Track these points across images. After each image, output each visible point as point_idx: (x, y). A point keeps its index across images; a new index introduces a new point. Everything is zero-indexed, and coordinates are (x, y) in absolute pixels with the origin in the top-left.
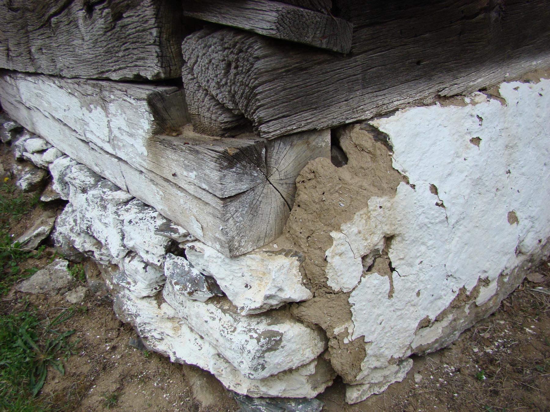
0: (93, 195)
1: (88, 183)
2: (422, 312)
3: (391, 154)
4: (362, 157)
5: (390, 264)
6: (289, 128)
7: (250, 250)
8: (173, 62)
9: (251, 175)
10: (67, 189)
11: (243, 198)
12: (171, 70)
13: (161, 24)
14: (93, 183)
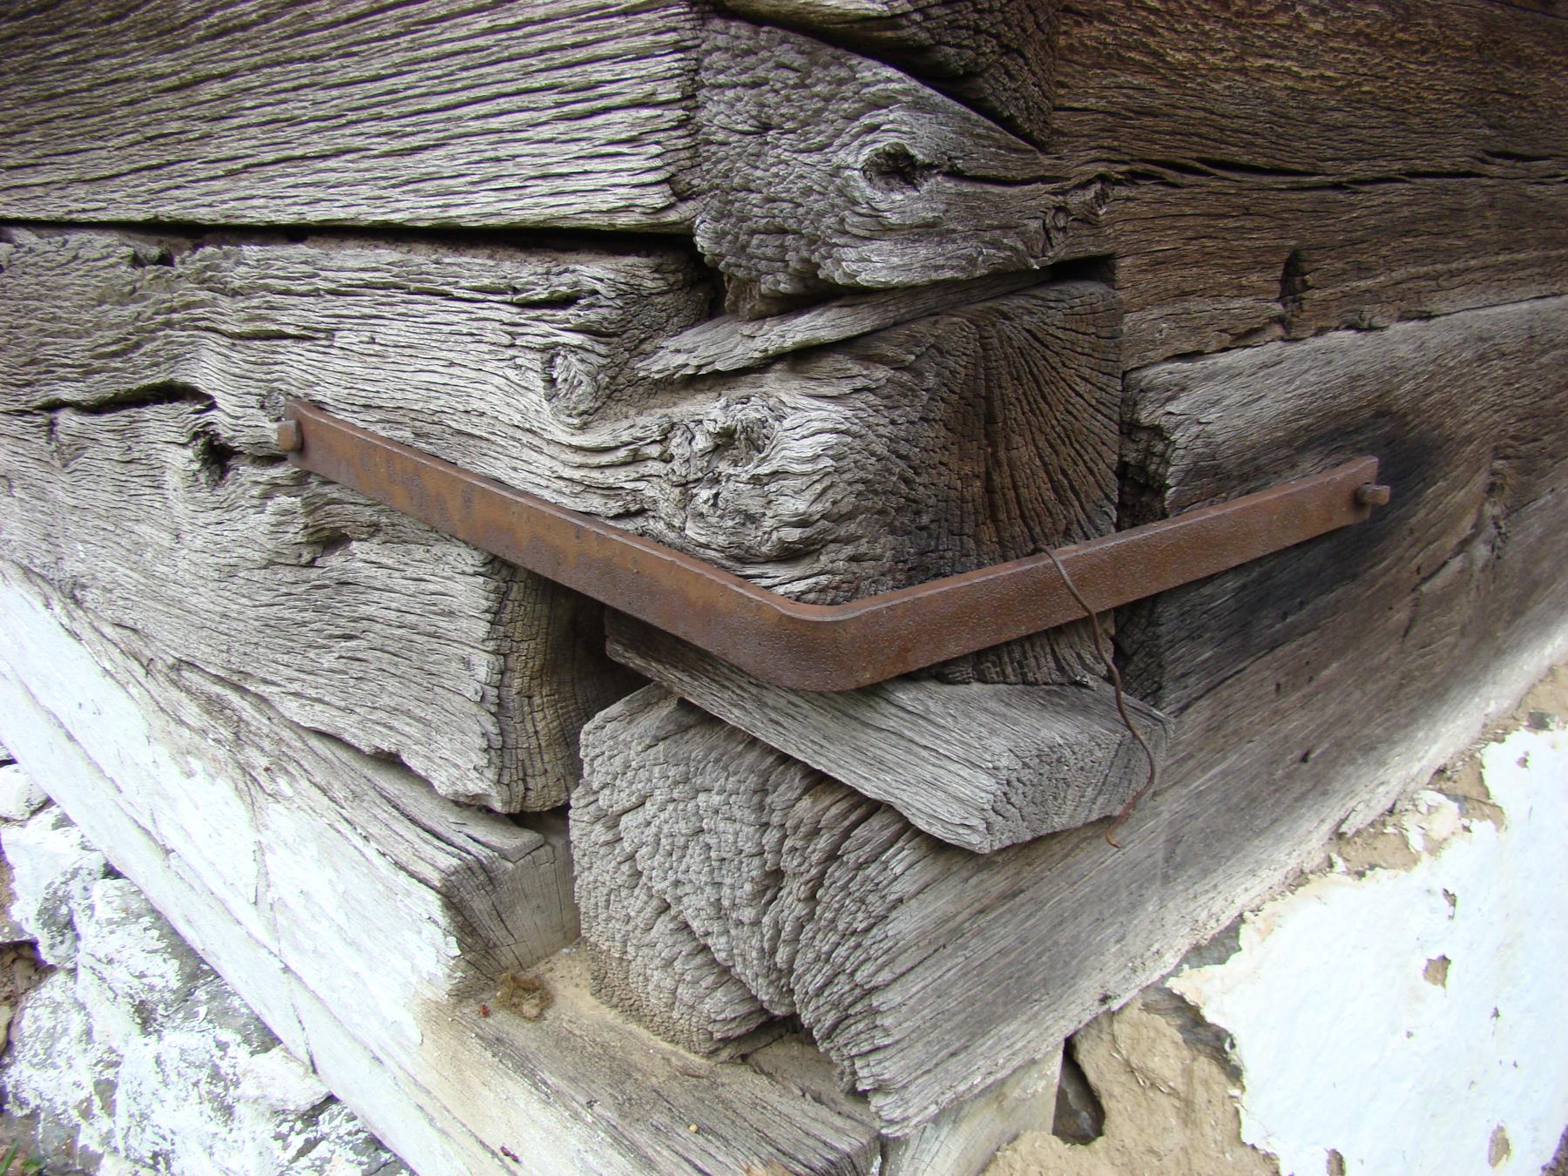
0: (183, 1051)
1: (159, 983)
3: (1236, 1092)
4: (1152, 1112)
8: (539, 765)
10: (68, 943)
12: (527, 789)
13: (507, 644)
14: (175, 984)
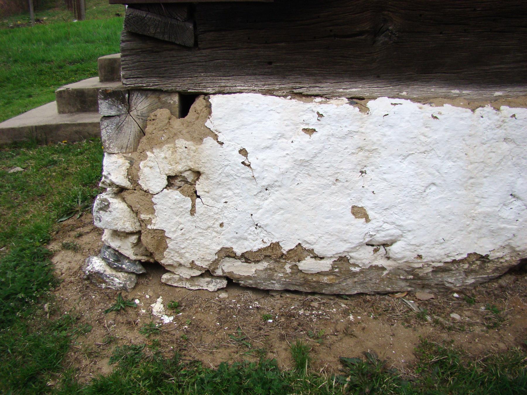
2: (225, 241)
5: (196, 192)
6: (140, 85)
7: (116, 152)
9: (118, 107)
11: (112, 119)
